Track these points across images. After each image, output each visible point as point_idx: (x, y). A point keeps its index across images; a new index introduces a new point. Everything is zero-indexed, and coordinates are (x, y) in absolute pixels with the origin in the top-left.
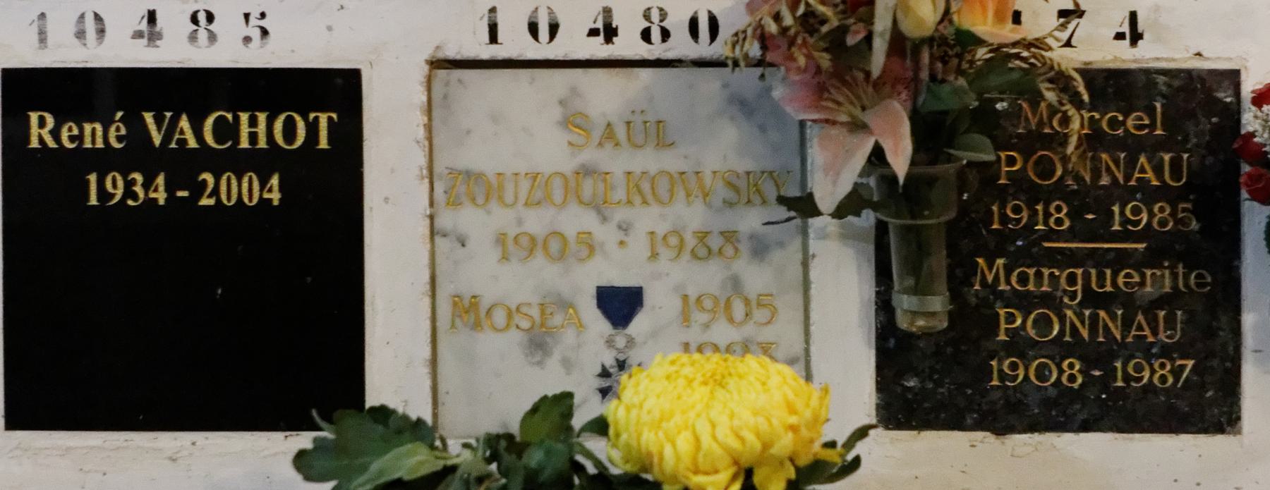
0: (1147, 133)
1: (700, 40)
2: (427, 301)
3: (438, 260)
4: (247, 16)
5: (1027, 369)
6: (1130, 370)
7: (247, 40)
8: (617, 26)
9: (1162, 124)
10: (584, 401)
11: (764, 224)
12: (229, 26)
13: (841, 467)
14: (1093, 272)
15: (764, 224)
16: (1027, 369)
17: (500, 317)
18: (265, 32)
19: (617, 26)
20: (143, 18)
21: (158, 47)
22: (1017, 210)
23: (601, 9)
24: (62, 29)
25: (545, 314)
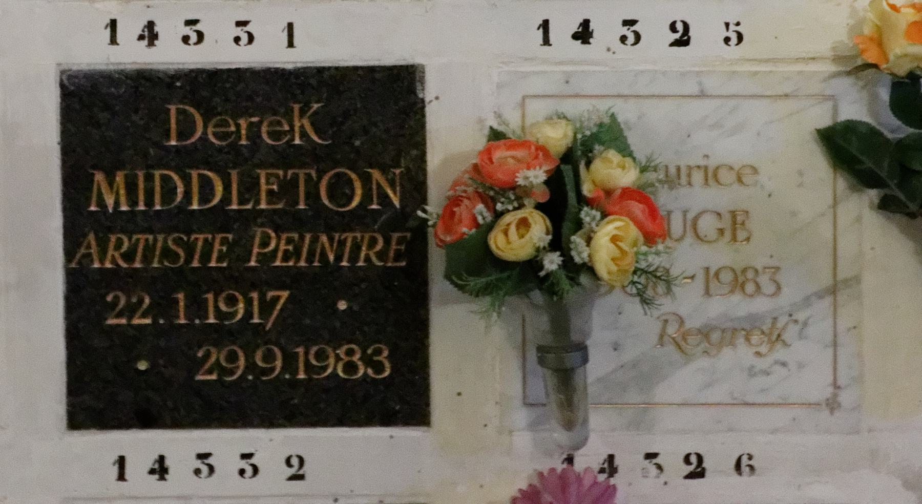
0: (329, 144)
1: (248, 20)
2: (616, 94)
3: (687, 93)
4: (727, 25)
5: (205, 133)
6: (223, 307)
8: (593, 30)
9: (185, 315)
10: (431, 101)
13: (247, 127)
14: (141, 174)
16: (205, 133)
17: (698, 177)
18: (740, 38)
19: (593, 30)
20: (284, 29)
21: (539, 28)
22: (232, 301)
23: (286, 25)
24: (129, 31)
25: (736, 224)
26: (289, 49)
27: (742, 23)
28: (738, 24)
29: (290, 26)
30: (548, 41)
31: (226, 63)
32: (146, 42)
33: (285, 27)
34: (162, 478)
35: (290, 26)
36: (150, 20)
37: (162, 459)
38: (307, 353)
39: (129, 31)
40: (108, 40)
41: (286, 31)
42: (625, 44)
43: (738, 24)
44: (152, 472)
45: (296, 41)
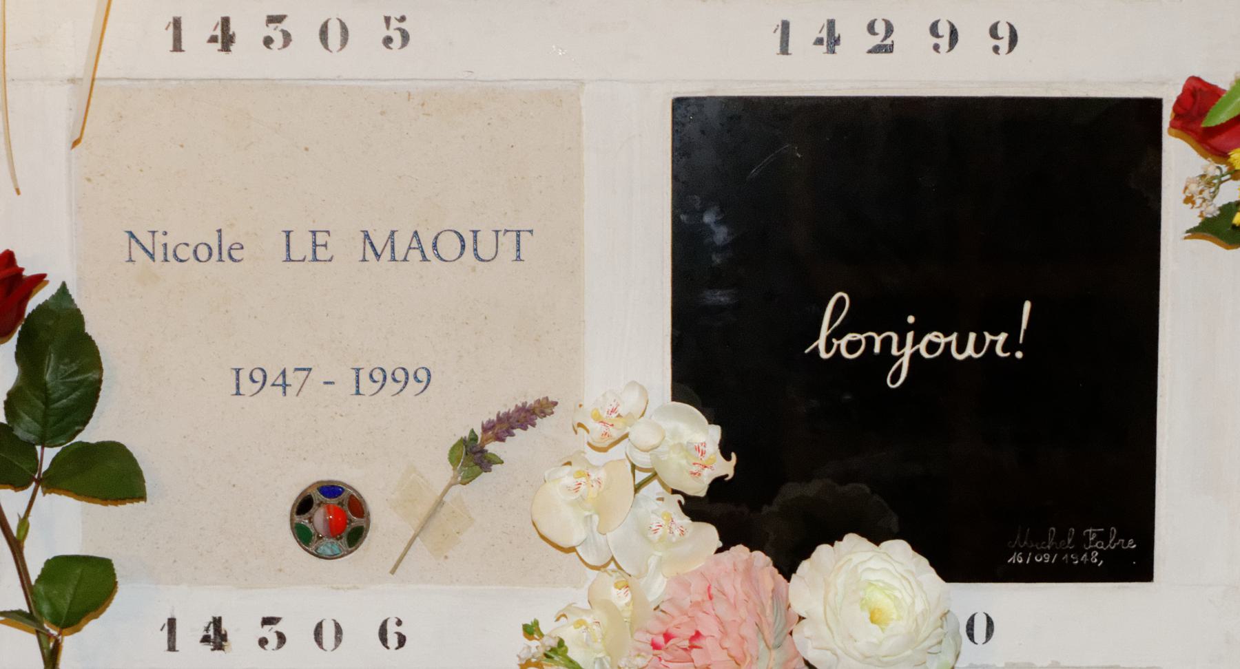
7: (388, 41)
11: (870, 52)
12: (974, 38)
15: (870, 52)
18: (405, 37)
20: (169, 25)
26: (175, 53)
27: (408, 18)
28: (403, 19)
29: (177, 23)
30: (787, 50)
31: (699, 92)
32: (219, 45)
33: (170, 23)
34: (219, 647)
35: (785, 26)
36: (785, 19)
37: (217, 622)
38: (1017, 554)
39: (855, 39)
40: (170, 46)
41: (779, 32)
42: (269, 47)
43: (403, 19)
44: (206, 639)
45: (185, 44)
